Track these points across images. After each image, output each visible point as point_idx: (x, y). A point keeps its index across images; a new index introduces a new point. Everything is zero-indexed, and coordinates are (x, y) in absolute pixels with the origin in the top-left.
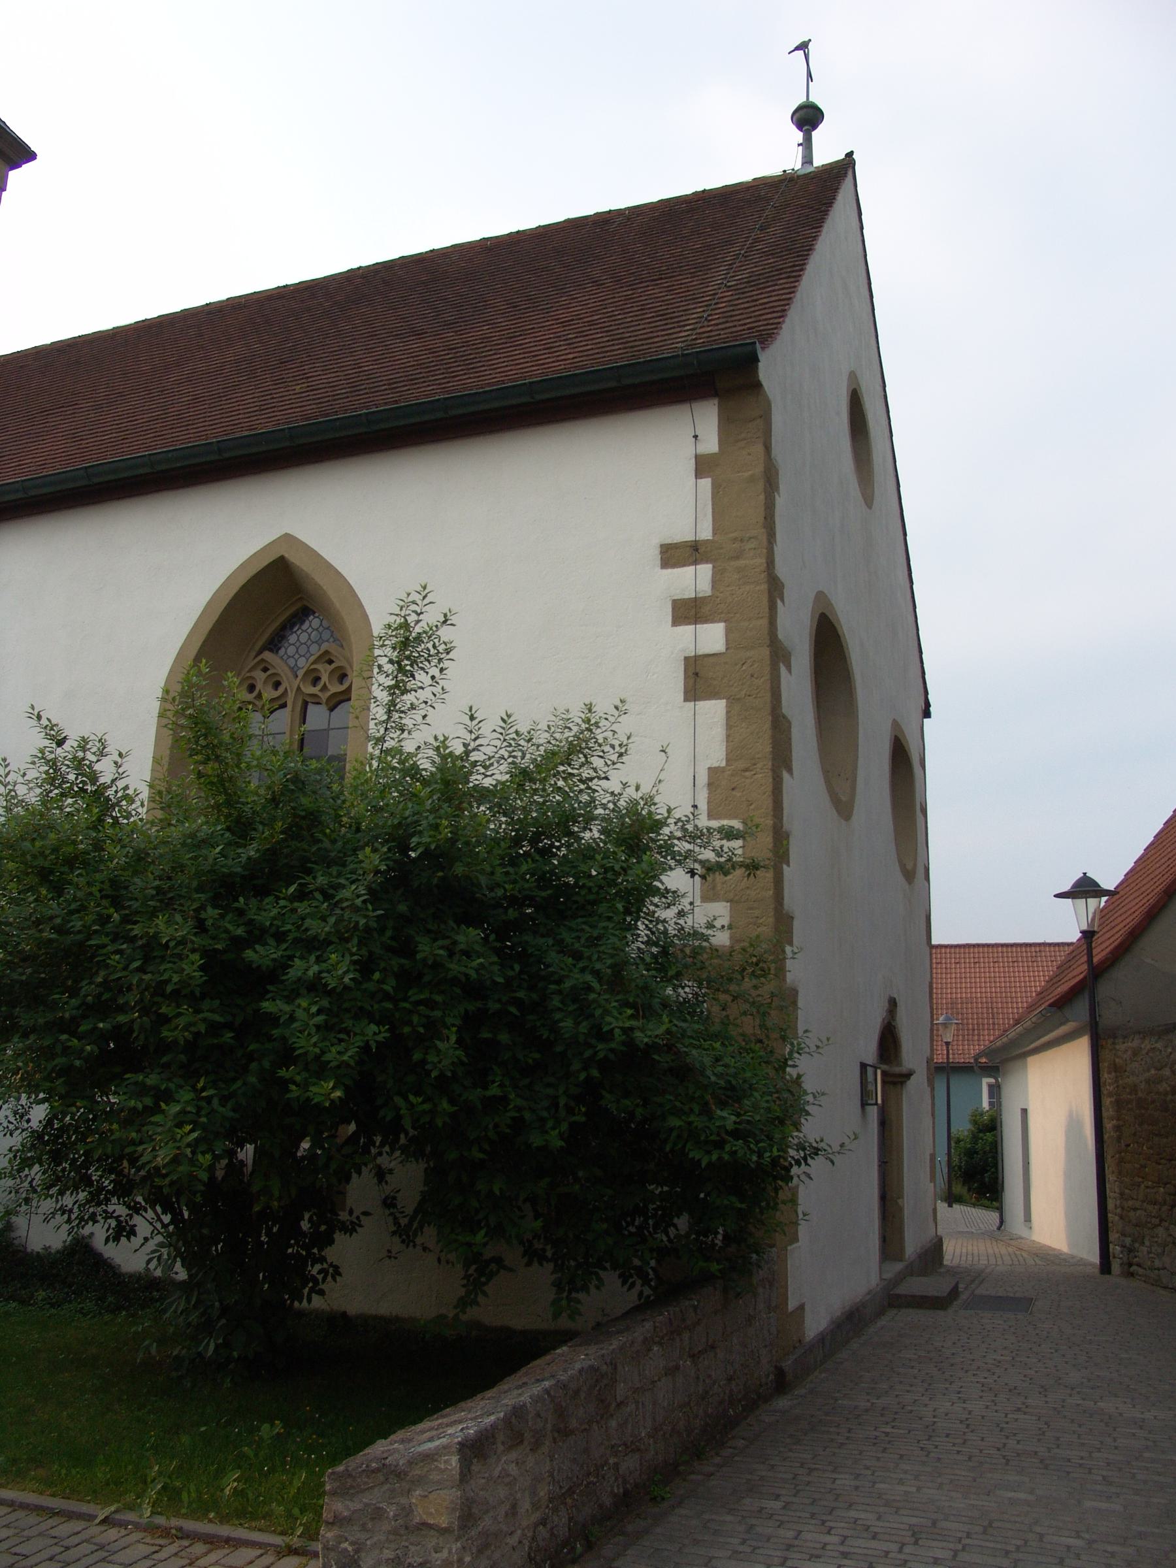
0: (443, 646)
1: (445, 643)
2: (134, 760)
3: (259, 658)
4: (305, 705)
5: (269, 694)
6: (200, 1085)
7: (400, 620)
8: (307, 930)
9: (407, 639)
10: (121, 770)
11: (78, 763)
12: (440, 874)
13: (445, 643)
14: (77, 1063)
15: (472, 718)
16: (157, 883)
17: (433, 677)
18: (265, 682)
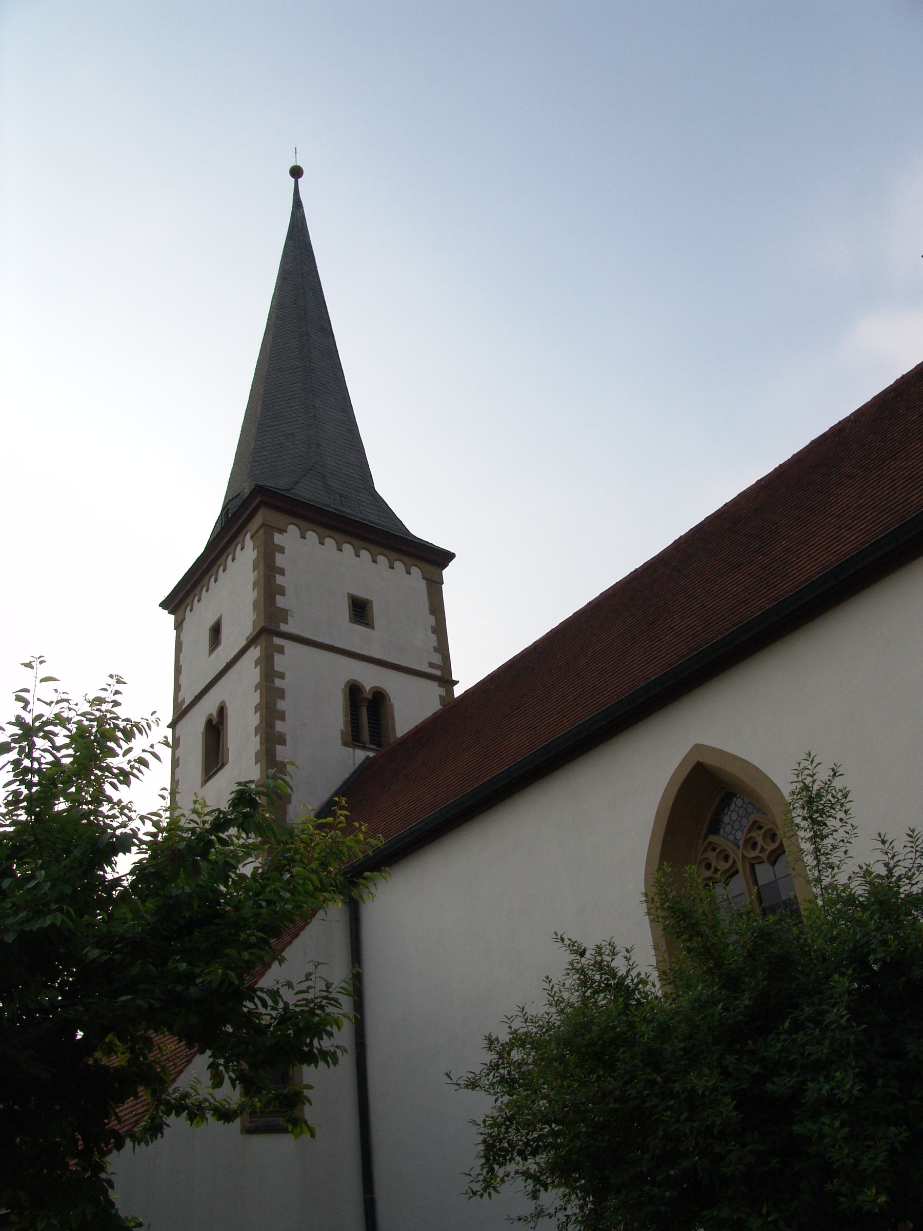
0: (840, 794)
1: (841, 791)
2: (639, 952)
3: (706, 842)
4: (752, 866)
5: (723, 866)
6: (764, 1211)
7: (801, 785)
8: (810, 1055)
9: (810, 797)
10: (631, 963)
11: (599, 966)
12: (903, 979)
13: (841, 791)
14: (663, 1208)
15: (883, 842)
16: (682, 1045)
17: (841, 820)
18: (717, 857)
